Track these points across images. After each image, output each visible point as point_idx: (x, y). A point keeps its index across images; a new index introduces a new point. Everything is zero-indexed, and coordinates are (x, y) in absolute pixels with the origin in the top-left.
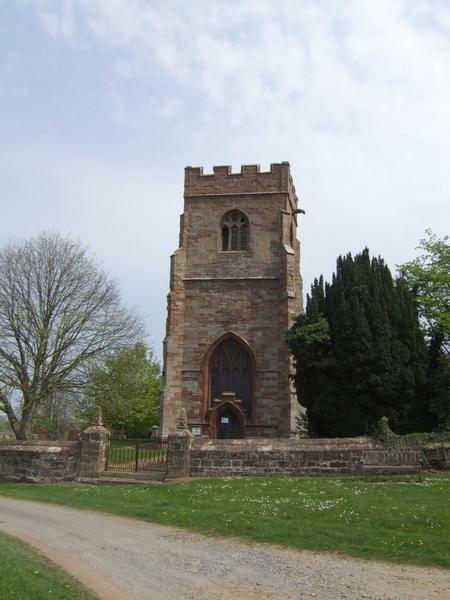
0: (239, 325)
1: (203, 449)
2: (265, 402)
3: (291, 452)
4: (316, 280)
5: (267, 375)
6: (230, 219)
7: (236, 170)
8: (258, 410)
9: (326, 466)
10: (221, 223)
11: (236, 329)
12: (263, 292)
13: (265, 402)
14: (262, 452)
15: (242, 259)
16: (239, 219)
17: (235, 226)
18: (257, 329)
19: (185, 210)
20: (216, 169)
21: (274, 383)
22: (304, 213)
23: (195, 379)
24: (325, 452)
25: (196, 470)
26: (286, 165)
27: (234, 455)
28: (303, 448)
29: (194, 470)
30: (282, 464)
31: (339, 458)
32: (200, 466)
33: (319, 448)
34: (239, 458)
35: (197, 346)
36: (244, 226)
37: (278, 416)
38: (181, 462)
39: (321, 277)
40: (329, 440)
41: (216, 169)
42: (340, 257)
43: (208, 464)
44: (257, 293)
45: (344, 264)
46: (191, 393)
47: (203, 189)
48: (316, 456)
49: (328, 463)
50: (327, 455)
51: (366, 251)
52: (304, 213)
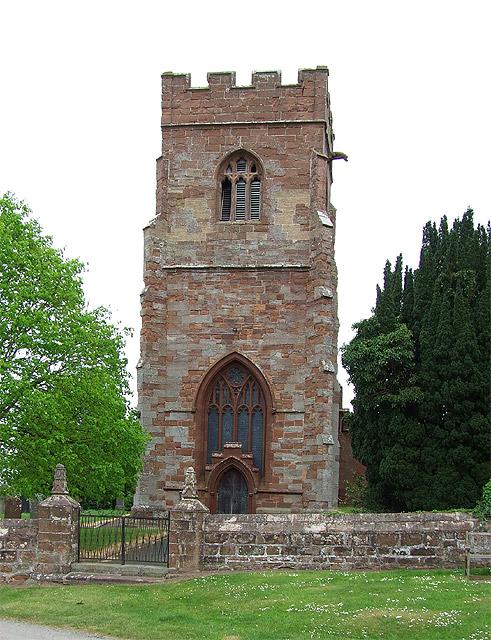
0: (249, 342)
1: (223, 528)
2: (285, 457)
3: (354, 534)
4: (388, 264)
5: (290, 418)
6: (234, 164)
7: (243, 80)
8: (275, 469)
9: (405, 554)
10: (219, 172)
11: (245, 347)
12: (284, 289)
13: (285, 457)
14: (312, 533)
15: (251, 236)
16: (248, 168)
17: (241, 179)
18: (273, 347)
19: (164, 148)
20: (212, 77)
21: (299, 429)
22: (344, 157)
23: (184, 424)
24: (405, 534)
25: (213, 560)
26: (324, 71)
27: (269, 538)
28: (372, 526)
29: (207, 562)
30: (340, 550)
31: (425, 542)
32: (218, 555)
33: (396, 527)
34: (276, 542)
35: (186, 374)
36: (256, 179)
37: (303, 477)
38: (191, 549)
39: (399, 258)
40: (409, 516)
41: (212, 77)
42: (429, 224)
43: (230, 551)
44: (275, 290)
45: (433, 237)
46: (178, 445)
47: (187, 114)
48: (390, 539)
49: (408, 549)
50: (407, 538)
51: (470, 213)
52: (344, 157)
